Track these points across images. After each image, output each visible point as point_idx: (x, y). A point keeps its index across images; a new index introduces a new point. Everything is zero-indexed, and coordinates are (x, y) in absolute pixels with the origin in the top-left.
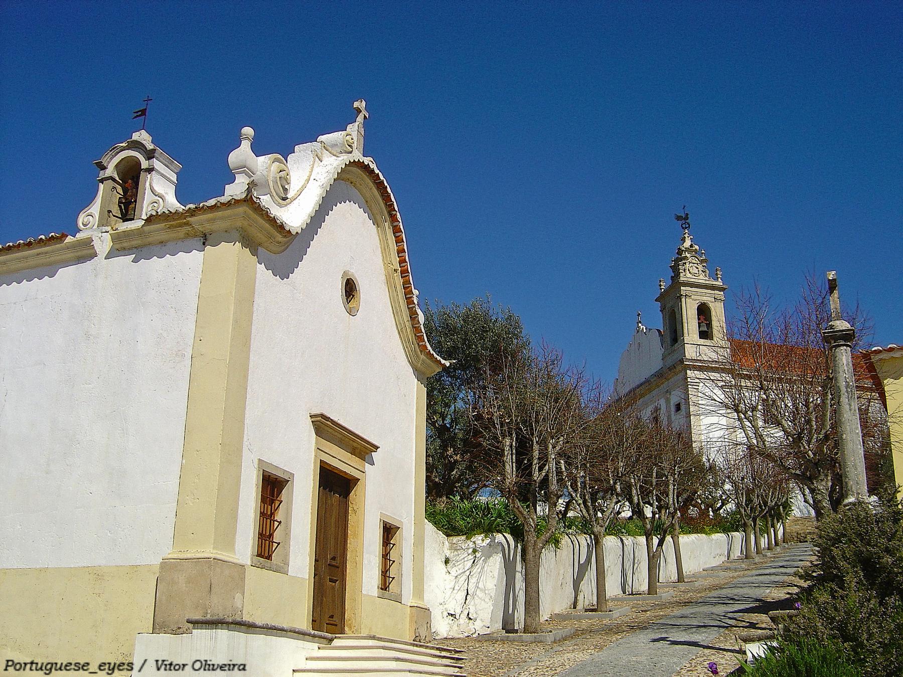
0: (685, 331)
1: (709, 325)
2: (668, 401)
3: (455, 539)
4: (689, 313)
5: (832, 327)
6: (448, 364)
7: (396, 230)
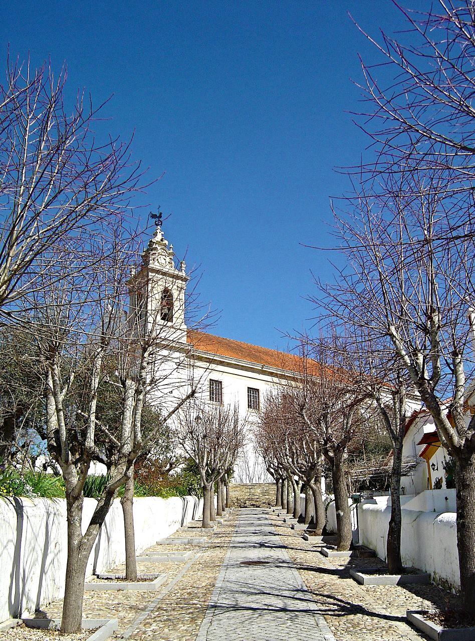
1: (170, 308)
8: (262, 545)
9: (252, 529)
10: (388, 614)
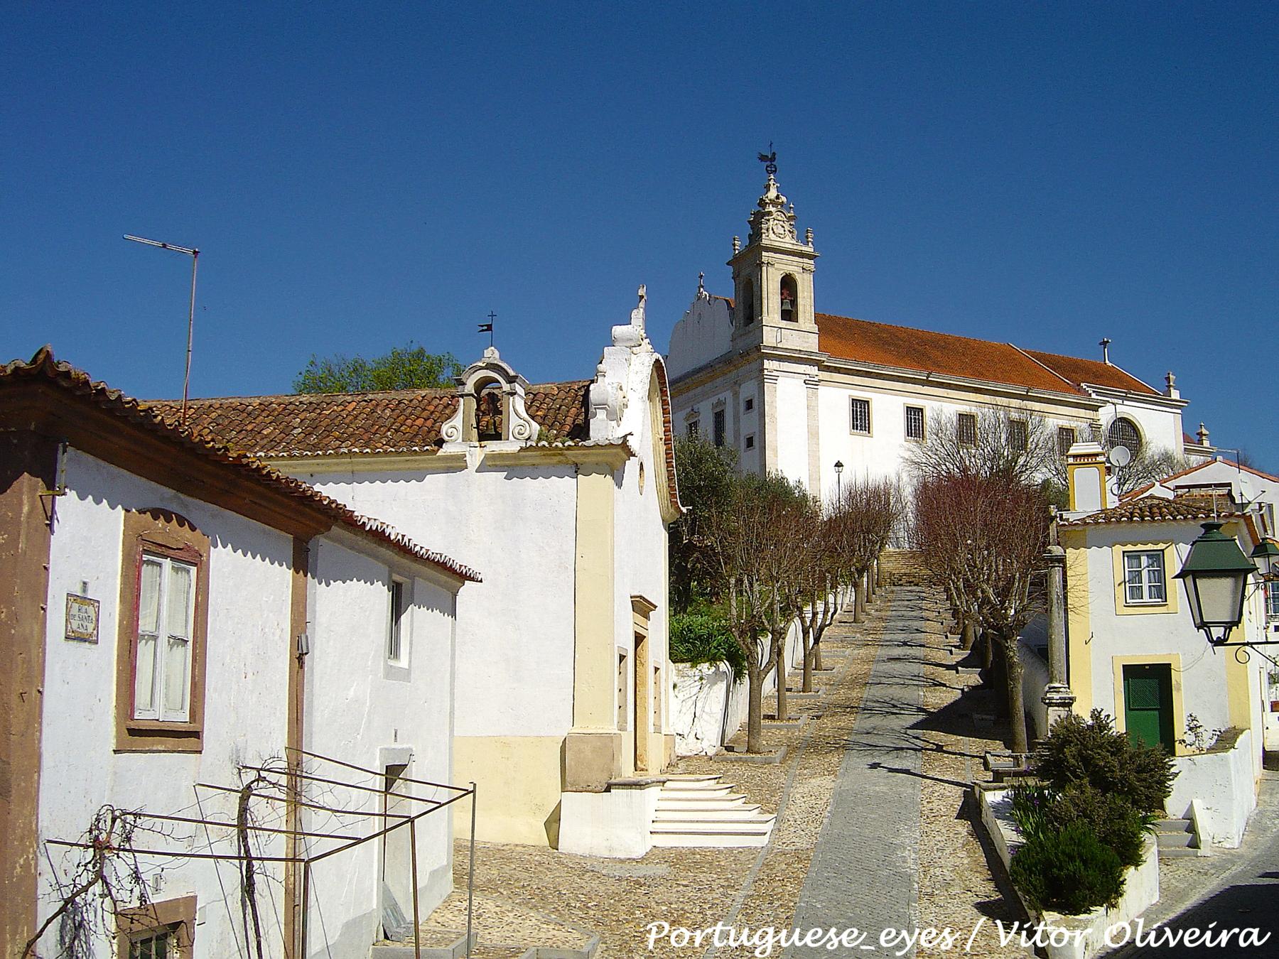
0: (765, 309)
1: (794, 303)
2: (736, 394)
3: (681, 666)
4: (771, 287)
5: (1050, 552)
6: (684, 510)
7: (664, 403)
8: (905, 644)
9: (900, 624)
10: (448, 675)
